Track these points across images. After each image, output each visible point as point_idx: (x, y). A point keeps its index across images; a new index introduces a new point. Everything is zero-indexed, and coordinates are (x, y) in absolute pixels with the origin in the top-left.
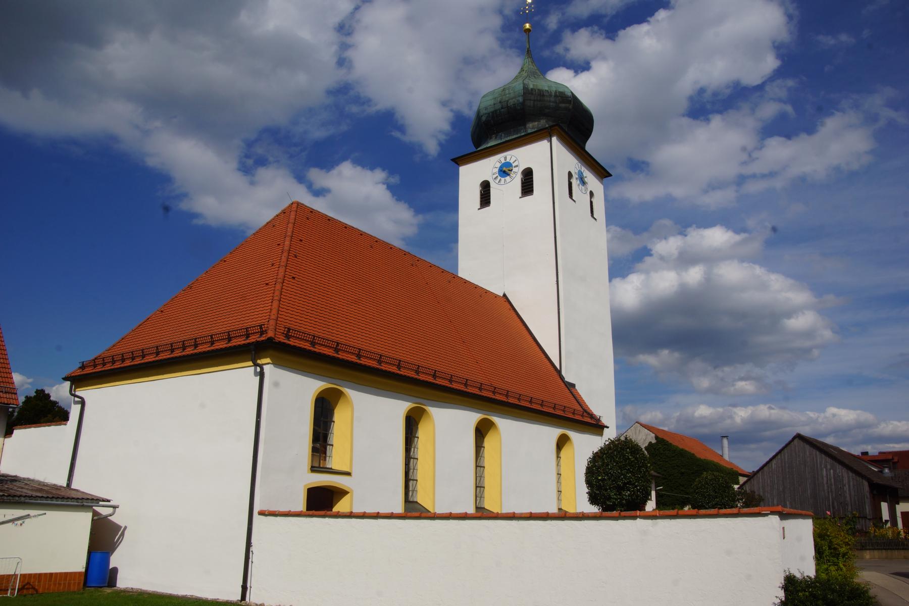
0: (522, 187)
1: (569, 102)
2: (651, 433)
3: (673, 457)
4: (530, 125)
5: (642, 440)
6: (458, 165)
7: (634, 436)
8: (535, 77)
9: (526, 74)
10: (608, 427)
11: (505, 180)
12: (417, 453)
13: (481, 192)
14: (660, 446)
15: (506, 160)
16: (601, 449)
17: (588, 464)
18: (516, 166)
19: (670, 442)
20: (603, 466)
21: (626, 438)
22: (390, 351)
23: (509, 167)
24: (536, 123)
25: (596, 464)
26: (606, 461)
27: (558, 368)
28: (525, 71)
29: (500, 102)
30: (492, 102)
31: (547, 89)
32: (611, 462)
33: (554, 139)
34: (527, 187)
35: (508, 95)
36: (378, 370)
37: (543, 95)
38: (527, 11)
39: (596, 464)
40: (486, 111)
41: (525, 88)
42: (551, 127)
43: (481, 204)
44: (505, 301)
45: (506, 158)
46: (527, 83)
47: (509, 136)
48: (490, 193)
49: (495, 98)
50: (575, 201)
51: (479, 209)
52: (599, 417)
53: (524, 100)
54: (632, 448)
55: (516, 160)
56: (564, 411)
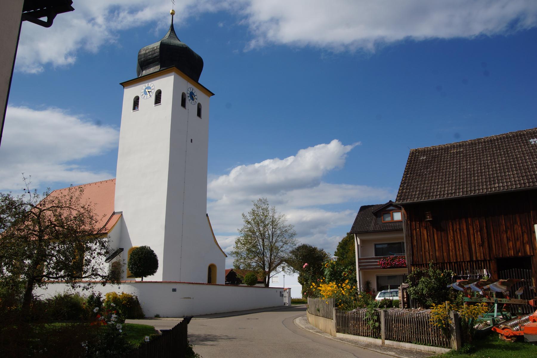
34: (158, 100)
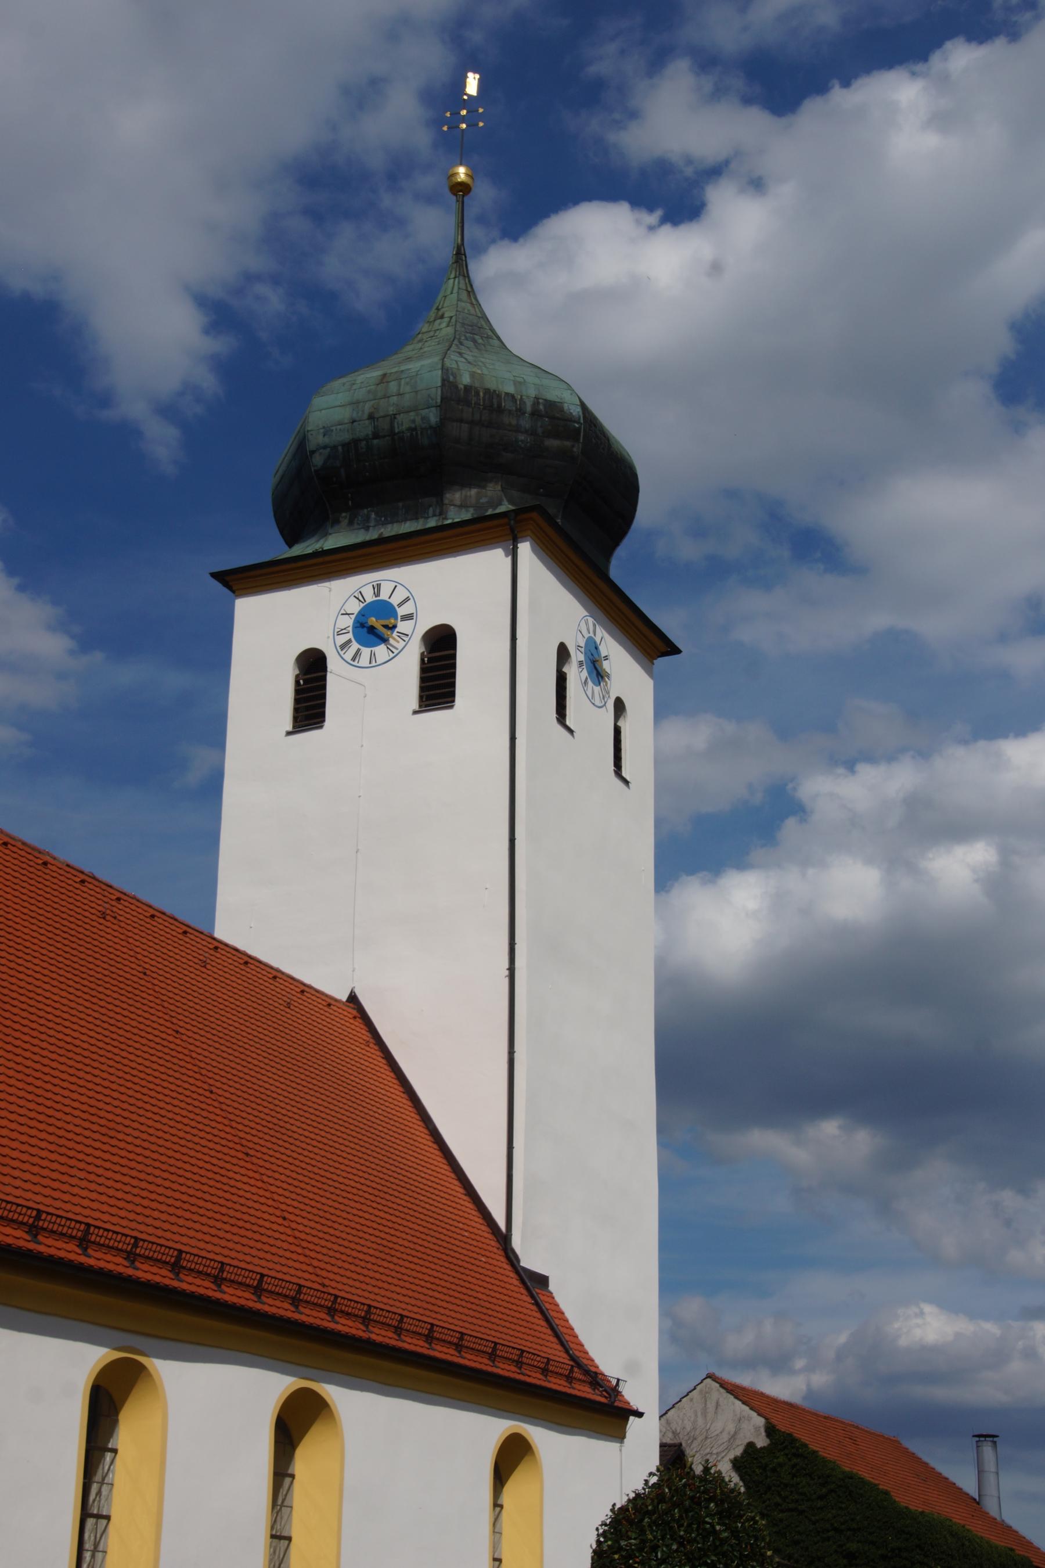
0: (423, 680)
1: (574, 435)
2: (754, 1414)
3: (821, 1498)
4: (456, 496)
5: (725, 1437)
6: (234, 592)
7: (700, 1421)
8: (475, 341)
9: (450, 330)
10: (640, 1415)
11: (373, 655)
12: (109, 1506)
13: (297, 682)
14: (781, 1460)
15: (377, 594)
16: (634, 1499)
17: (598, 1542)
18: (408, 617)
19: (813, 1447)
20: (641, 1550)
21: (706, 1470)
22: (56, 1194)
23: (389, 618)
24: (474, 492)
25: (623, 1543)
26: (650, 1537)
27: (502, 1224)
28: (446, 320)
29: (371, 417)
30: (346, 414)
31: (510, 389)
32: (663, 1538)
33: (525, 549)
35: (394, 399)
36: (28, 1254)
37: (500, 410)
38: (464, 126)
39: (623, 1543)
40: (327, 440)
41: (448, 383)
42: (517, 512)
43: (295, 719)
44: (355, 1017)
45: (377, 591)
46: (454, 366)
47: (392, 522)
48: (324, 687)
49: (358, 402)
50: (571, 731)
51: (289, 733)
52: (614, 1382)
53: (443, 421)
54: (722, 1501)
55: (407, 599)
56: (519, 1364)
